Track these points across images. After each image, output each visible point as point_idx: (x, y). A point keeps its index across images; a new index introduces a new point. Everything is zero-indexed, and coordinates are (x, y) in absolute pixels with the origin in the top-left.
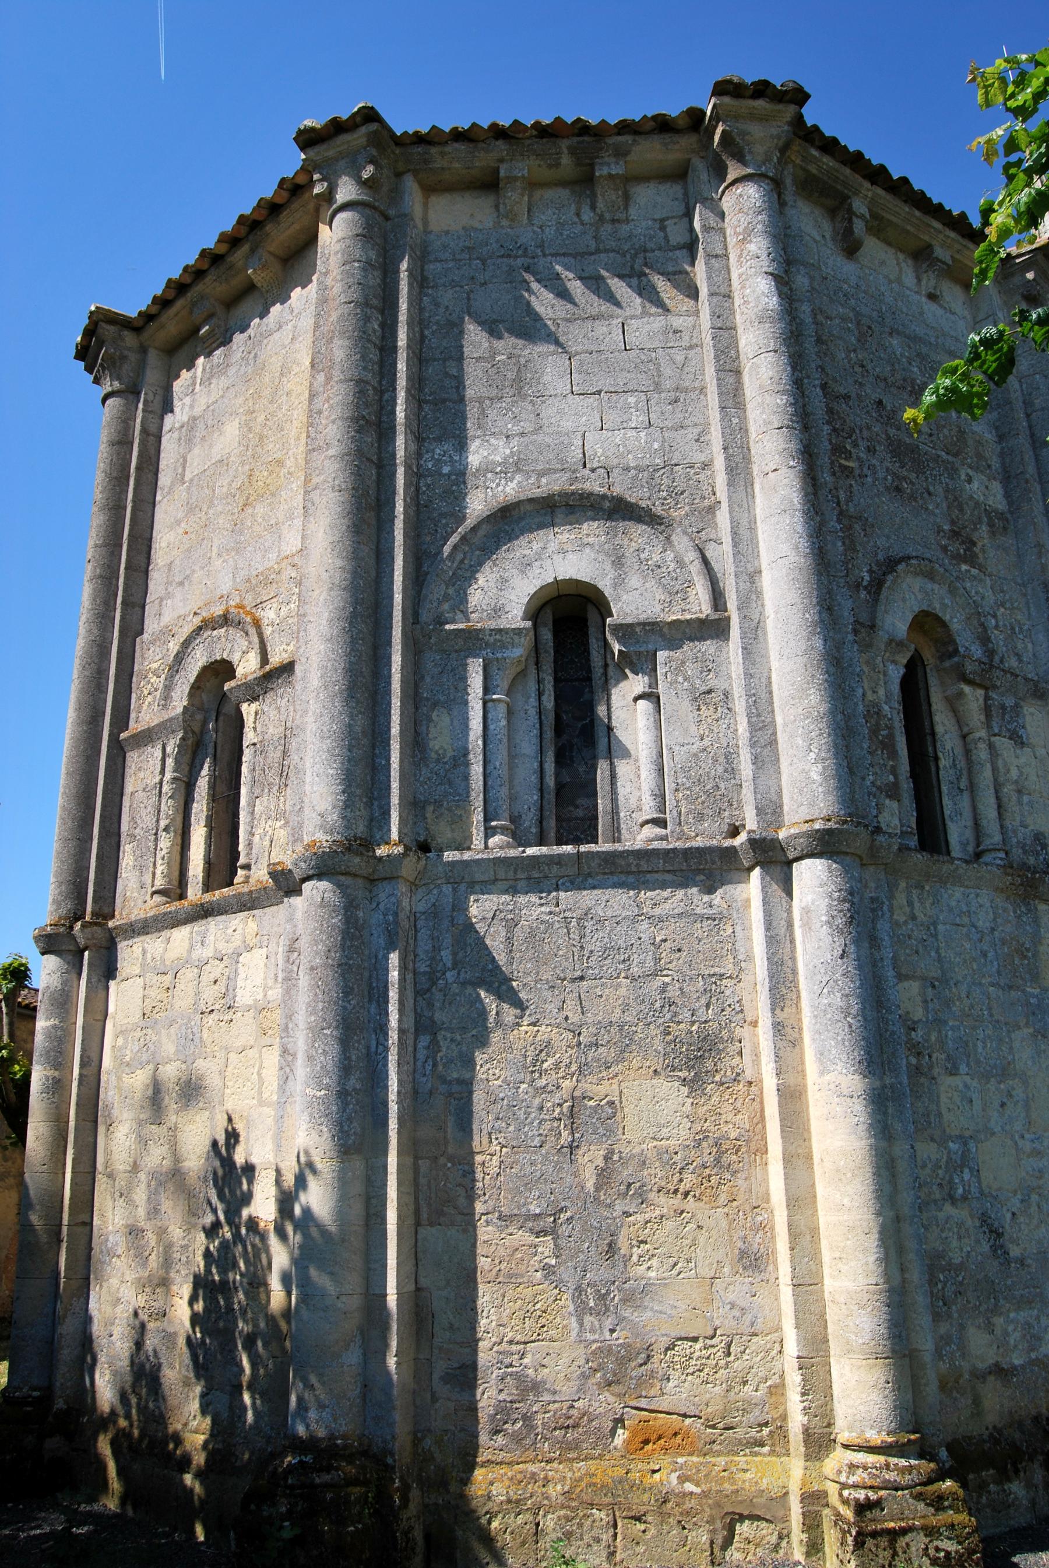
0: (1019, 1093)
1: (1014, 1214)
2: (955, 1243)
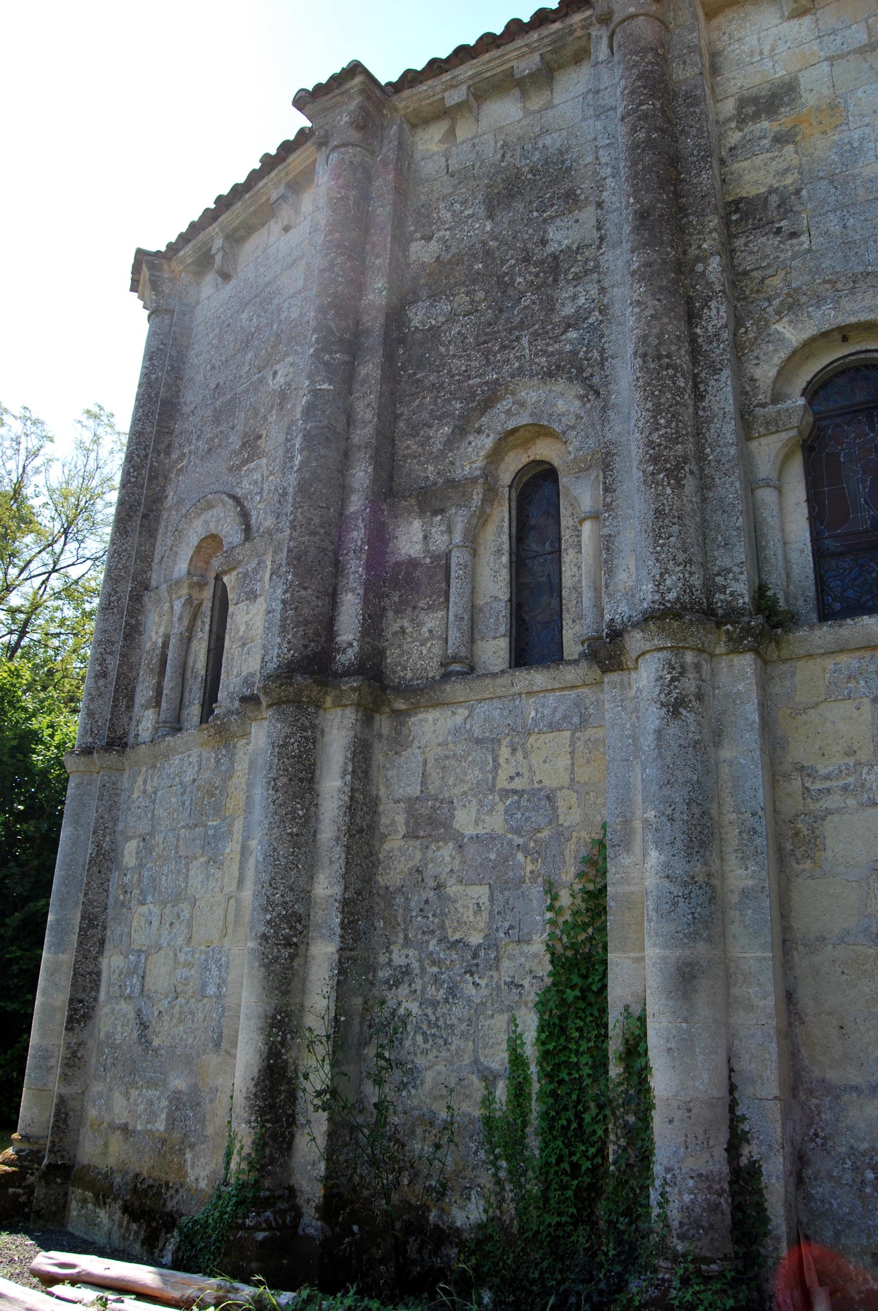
0: (186, 914)
1: (160, 1012)
2: (119, 1029)
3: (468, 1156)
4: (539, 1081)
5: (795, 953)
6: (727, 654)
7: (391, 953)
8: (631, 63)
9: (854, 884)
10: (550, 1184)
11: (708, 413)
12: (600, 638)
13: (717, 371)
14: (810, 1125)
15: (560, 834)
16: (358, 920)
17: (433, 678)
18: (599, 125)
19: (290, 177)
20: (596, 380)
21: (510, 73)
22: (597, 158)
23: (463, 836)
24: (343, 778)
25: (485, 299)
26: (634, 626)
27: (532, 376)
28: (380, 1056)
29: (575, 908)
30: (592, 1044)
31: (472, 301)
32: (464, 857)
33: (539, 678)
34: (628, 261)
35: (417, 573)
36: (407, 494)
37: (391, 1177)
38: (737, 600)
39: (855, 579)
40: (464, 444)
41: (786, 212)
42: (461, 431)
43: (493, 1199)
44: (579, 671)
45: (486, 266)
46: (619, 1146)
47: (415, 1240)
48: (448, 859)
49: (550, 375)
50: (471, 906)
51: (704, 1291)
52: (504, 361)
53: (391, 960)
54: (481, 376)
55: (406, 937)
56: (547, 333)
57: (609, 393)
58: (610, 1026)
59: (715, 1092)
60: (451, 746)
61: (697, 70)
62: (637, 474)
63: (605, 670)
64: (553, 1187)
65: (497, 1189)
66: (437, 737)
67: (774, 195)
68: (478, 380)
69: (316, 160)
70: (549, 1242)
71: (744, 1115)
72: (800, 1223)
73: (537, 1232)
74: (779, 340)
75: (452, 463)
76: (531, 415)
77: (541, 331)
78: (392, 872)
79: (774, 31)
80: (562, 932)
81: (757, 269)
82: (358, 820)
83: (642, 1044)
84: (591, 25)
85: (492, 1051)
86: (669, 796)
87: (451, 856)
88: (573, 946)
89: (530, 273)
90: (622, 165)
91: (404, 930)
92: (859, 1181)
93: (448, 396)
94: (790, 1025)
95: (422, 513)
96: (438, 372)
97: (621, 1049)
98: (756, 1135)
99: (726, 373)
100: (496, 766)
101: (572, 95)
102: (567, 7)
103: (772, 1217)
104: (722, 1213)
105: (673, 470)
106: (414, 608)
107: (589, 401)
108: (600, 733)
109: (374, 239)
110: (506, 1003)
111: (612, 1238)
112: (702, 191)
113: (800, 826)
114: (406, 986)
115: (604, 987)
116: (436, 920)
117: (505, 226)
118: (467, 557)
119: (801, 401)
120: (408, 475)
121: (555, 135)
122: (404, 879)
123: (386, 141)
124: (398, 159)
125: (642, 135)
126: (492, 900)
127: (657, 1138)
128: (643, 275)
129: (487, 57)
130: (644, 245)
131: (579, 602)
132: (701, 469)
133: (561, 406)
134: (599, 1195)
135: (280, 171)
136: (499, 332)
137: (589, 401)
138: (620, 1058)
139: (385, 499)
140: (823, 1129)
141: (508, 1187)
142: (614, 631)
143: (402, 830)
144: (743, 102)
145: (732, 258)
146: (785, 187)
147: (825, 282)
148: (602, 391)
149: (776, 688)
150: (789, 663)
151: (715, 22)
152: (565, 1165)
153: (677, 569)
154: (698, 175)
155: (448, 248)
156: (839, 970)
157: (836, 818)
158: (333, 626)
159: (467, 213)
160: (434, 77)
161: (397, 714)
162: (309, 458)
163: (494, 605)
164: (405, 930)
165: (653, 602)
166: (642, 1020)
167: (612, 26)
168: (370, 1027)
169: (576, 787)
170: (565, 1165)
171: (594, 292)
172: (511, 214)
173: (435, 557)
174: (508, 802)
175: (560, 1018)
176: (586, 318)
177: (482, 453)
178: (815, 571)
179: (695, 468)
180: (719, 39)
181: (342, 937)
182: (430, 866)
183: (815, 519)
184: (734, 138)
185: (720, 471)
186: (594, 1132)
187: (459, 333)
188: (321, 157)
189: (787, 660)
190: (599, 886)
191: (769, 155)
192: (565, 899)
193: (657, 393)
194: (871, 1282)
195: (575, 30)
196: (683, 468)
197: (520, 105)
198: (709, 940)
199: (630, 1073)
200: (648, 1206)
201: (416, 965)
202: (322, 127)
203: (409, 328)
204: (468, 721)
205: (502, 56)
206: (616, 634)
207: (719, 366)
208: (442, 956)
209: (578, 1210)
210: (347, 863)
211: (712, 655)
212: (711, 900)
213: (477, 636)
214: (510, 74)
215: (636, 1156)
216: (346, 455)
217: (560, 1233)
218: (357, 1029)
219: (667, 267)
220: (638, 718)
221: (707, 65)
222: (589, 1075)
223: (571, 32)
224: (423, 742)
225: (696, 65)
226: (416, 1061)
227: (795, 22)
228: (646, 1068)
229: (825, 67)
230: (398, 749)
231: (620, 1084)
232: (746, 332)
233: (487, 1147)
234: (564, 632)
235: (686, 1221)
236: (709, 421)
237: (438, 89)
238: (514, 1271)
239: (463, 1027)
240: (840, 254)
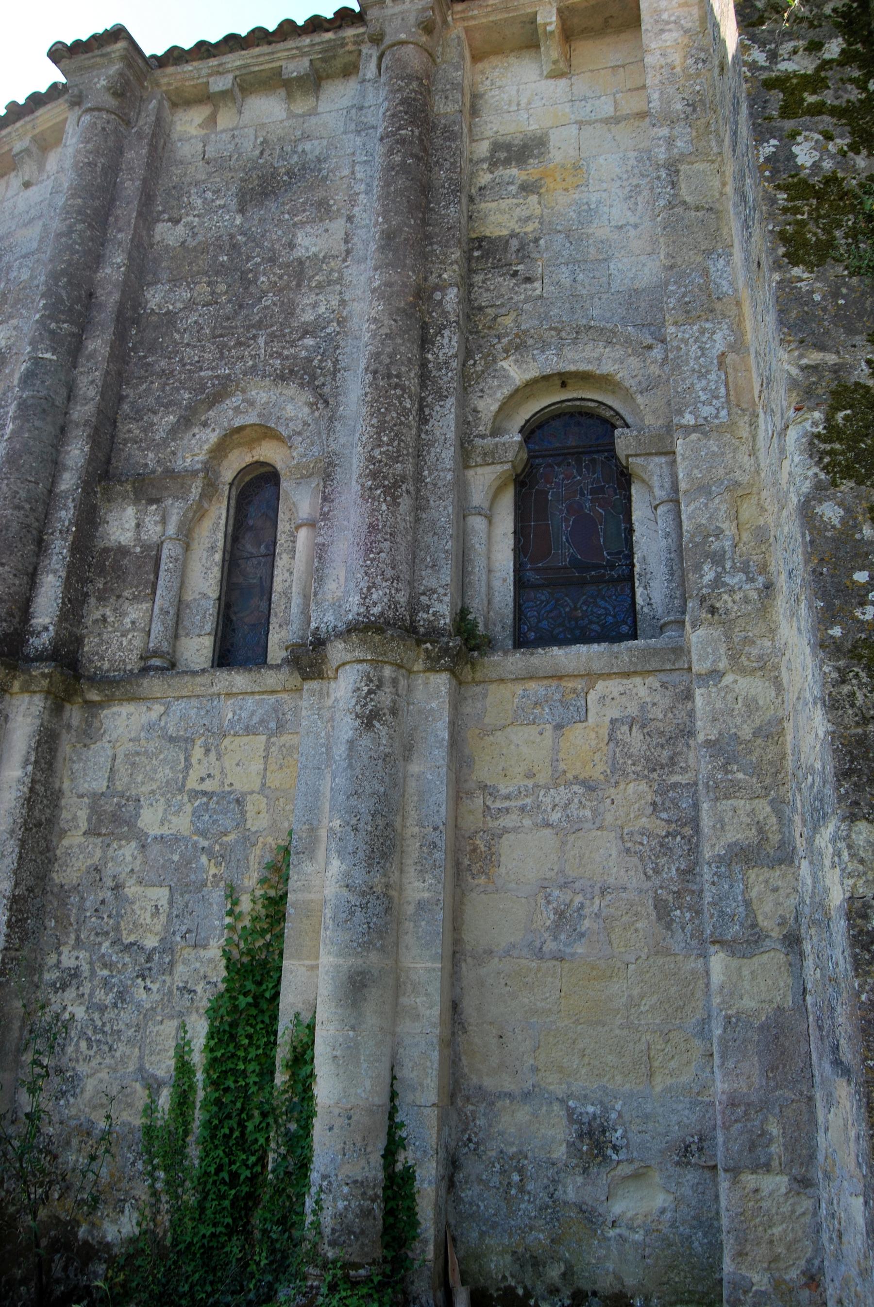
3: (125, 1166)
4: (204, 1089)
5: (463, 965)
6: (424, 671)
7: (60, 954)
8: (396, 87)
9: (523, 900)
10: (208, 1194)
11: (430, 437)
12: (304, 645)
13: (442, 397)
14: (464, 1131)
15: (246, 839)
16: (28, 918)
17: (131, 671)
18: (359, 141)
19: (37, 131)
20: (327, 390)
21: (278, 72)
22: (353, 173)
23: (147, 835)
24: (24, 768)
25: (226, 293)
26: (336, 636)
27: (264, 377)
28: (36, 1063)
29: (254, 914)
30: (260, 1051)
31: (213, 293)
32: (145, 857)
33: (239, 680)
34: (370, 278)
35: (126, 561)
36: (123, 479)
37: (40, 1191)
38: (439, 620)
39: (551, 611)
40: (189, 435)
41: (524, 257)
42: (186, 422)
43: (147, 1212)
44: (280, 676)
45: (231, 260)
46: (280, 1154)
47: (61, 1258)
48: (129, 858)
49: (282, 378)
50: (149, 908)
51: (351, 1296)
52: (238, 358)
53: (59, 962)
54: (213, 369)
55: (78, 938)
56: (284, 336)
57: (338, 405)
58: (280, 1034)
59: (376, 1099)
60: (143, 742)
61: (457, 107)
62: (355, 487)
63: (306, 678)
64: (210, 1198)
65: (153, 1200)
66: (129, 732)
67: (514, 239)
68: (210, 373)
69: (67, 118)
70: (202, 1254)
71: (402, 1122)
72: (448, 1225)
73: (191, 1244)
75: (174, 453)
76: (259, 416)
77: (278, 333)
78: (69, 870)
79: (533, 85)
80: (240, 938)
81: (492, 306)
82: (37, 813)
83: (308, 1052)
84: (362, 42)
85: (158, 1057)
86: (356, 806)
87: (132, 855)
88: (249, 952)
89: (275, 274)
90: (376, 183)
91: (76, 931)
92: (505, 1183)
93: (177, 384)
94: (453, 1034)
95: (137, 501)
96: (170, 358)
97: (289, 1056)
98: (412, 1141)
99: (451, 400)
100: (188, 766)
101: (336, 107)
102: (342, 19)
103: (422, 1221)
104: (374, 1219)
105: (390, 488)
106: (119, 597)
107: (318, 409)
108: (295, 740)
109: (119, 212)
110: (177, 1009)
111: (265, 1247)
112: (448, 223)
113: (478, 842)
114: (73, 989)
115: (277, 994)
116: (111, 922)
117: (256, 222)
118: (179, 550)
119: (518, 438)
120: (127, 459)
121: (316, 142)
122: (81, 878)
123: (143, 114)
124: (154, 135)
125: (398, 158)
126: (171, 902)
127: (316, 1146)
128: (379, 293)
129: (257, 50)
130: (388, 265)
131: (288, 608)
132: (418, 491)
133: (290, 410)
134: (256, 1205)
135: (26, 123)
136: (236, 327)
137: (318, 409)
138: (287, 1066)
139: (99, 481)
140: (476, 1134)
141: (164, 1198)
142: (319, 639)
143: (84, 826)
144: (496, 147)
145: (470, 292)
146: (526, 233)
147: (551, 329)
148: (331, 401)
149: (467, 709)
151: (480, 66)
152: (225, 1175)
153: (384, 584)
154: (447, 207)
155: (195, 235)
156: (503, 982)
157: (511, 836)
158: (29, 607)
159: (218, 202)
160: (201, 59)
161: (89, 704)
162: (21, 428)
163: (203, 602)
164: (78, 931)
165: (358, 614)
166: (311, 1028)
167: (382, 47)
168: (31, 1032)
169: (267, 792)
170: (225, 1175)
171: (334, 303)
172: (262, 212)
173: (145, 547)
174: (196, 804)
175: (231, 1025)
176: (324, 328)
177: (206, 447)
178: (515, 600)
179: (412, 489)
180: (482, 83)
181: (8, 935)
182: (110, 865)
183: (520, 550)
184: (485, 178)
185: (436, 494)
186: (256, 1140)
187: (195, 322)
188: (72, 116)
189: (481, 682)
190: (280, 893)
191: (515, 201)
192: (245, 905)
193: (383, 410)
194: (510, 1279)
195: (347, 44)
196: (400, 487)
197: (285, 106)
198: (382, 949)
199: (295, 1081)
200: (302, 1213)
201: (85, 967)
202: (76, 85)
203: (145, 309)
204: (163, 718)
205: (273, 53)
206: (319, 643)
207: (445, 393)
208: (114, 958)
209: (234, 1220)
210: (20, 858)
211: (410, 672)
212: (387, 910)
213: (181, 632)
214: (278, 72)
215: (295, 1164)
216: (63, 430)
217: (214, 1244)
218: (17, 1034)
219: (407, 290)
220: (333, 727)
221: (468, 105)
222: (255, 1083)
223: (343, 45)
224: (114, 736)
225: (457, 102)
226: (78, 1068)
227: (551, 82)
228: (312, 1075)
229: (574, 129)
230: (88, 741)
231: (285, 1091)
233: (146, 1157)
234: (270, 636)
235: (338, 1227)
236: (430, 444)
237: (204, 72)
238: (164, 1286)
239: (131, 1032)
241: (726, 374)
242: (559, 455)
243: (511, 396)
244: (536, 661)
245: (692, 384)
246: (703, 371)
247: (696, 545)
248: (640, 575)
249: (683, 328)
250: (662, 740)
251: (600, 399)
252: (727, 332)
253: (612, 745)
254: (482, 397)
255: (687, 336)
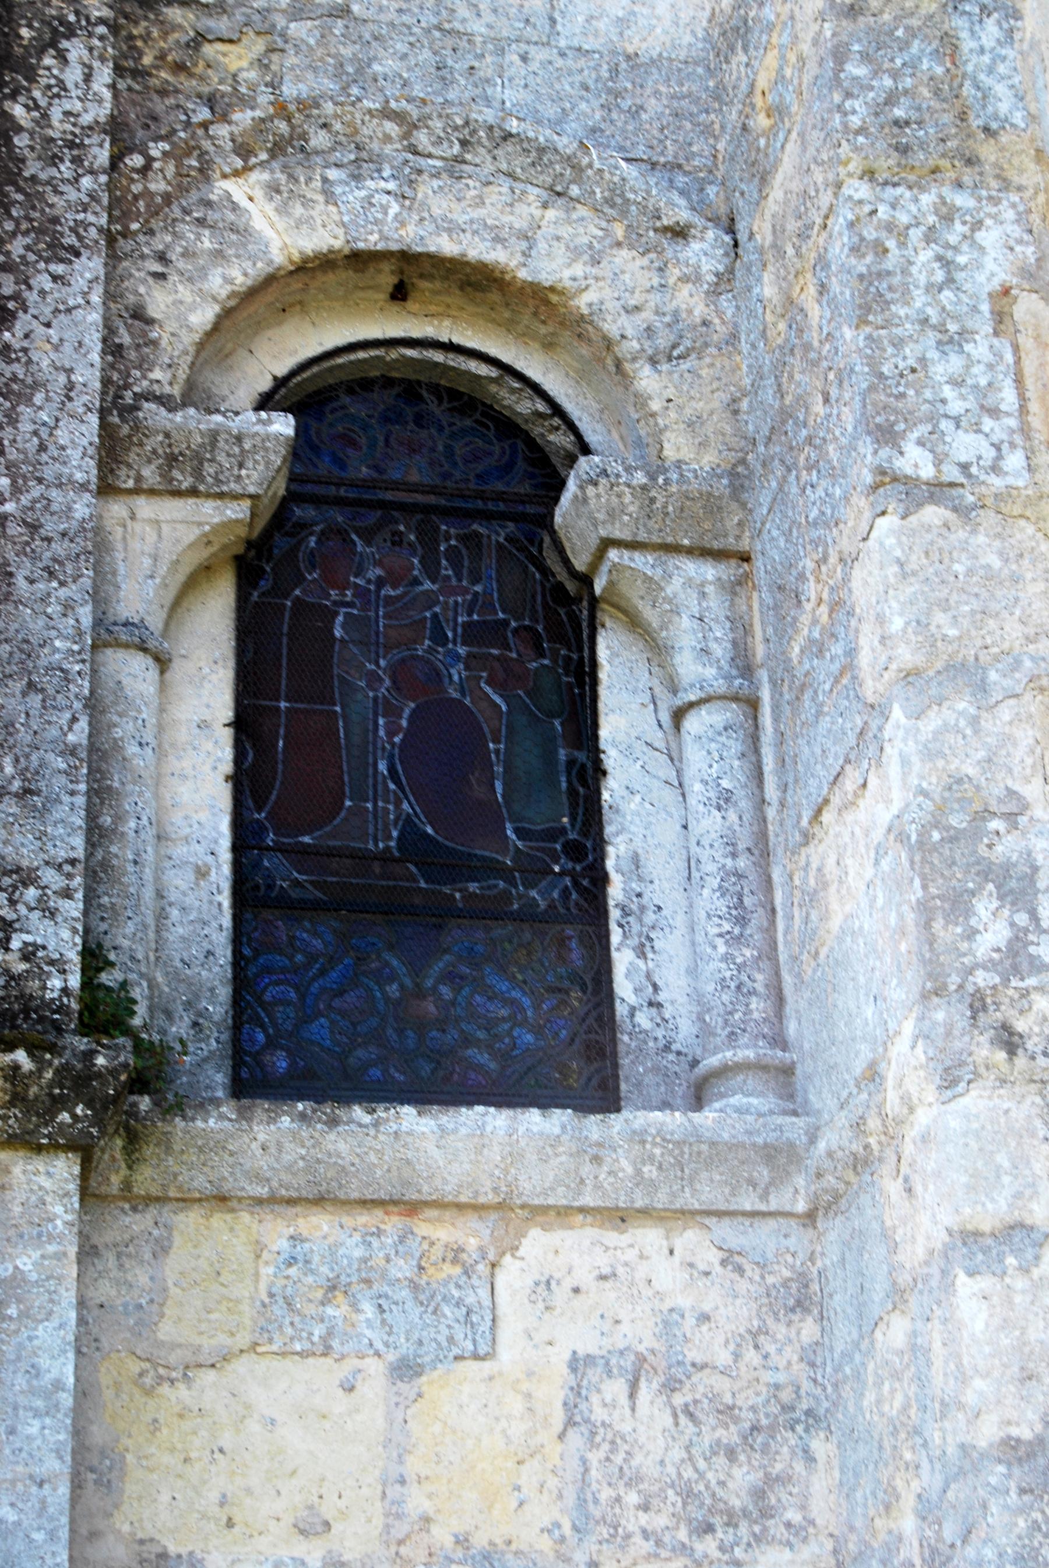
11: (19, 369)
74: (233, 229)
147: (387, 113)
150: (153, 1211)
189: (150, 1200)
207: (70, 240)
232: (145, 170)
240: (426, 54)
241: (1016, 348)
242: (371, 505)
243: (251, 294)
244: (342, 1146)
245: (923, 360)
246: (953, 327)
247: (953, 838)
248: (626, 912)
249: (890, 192)
250: (731, 1435)
251: (506, 358)
252: (1016, 231)
253: (576, 1439)
254: (161, 276)
255: (904, 218)
